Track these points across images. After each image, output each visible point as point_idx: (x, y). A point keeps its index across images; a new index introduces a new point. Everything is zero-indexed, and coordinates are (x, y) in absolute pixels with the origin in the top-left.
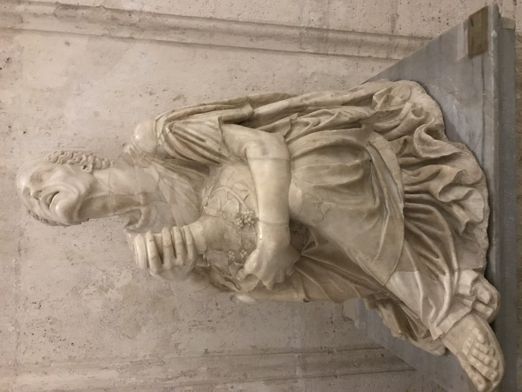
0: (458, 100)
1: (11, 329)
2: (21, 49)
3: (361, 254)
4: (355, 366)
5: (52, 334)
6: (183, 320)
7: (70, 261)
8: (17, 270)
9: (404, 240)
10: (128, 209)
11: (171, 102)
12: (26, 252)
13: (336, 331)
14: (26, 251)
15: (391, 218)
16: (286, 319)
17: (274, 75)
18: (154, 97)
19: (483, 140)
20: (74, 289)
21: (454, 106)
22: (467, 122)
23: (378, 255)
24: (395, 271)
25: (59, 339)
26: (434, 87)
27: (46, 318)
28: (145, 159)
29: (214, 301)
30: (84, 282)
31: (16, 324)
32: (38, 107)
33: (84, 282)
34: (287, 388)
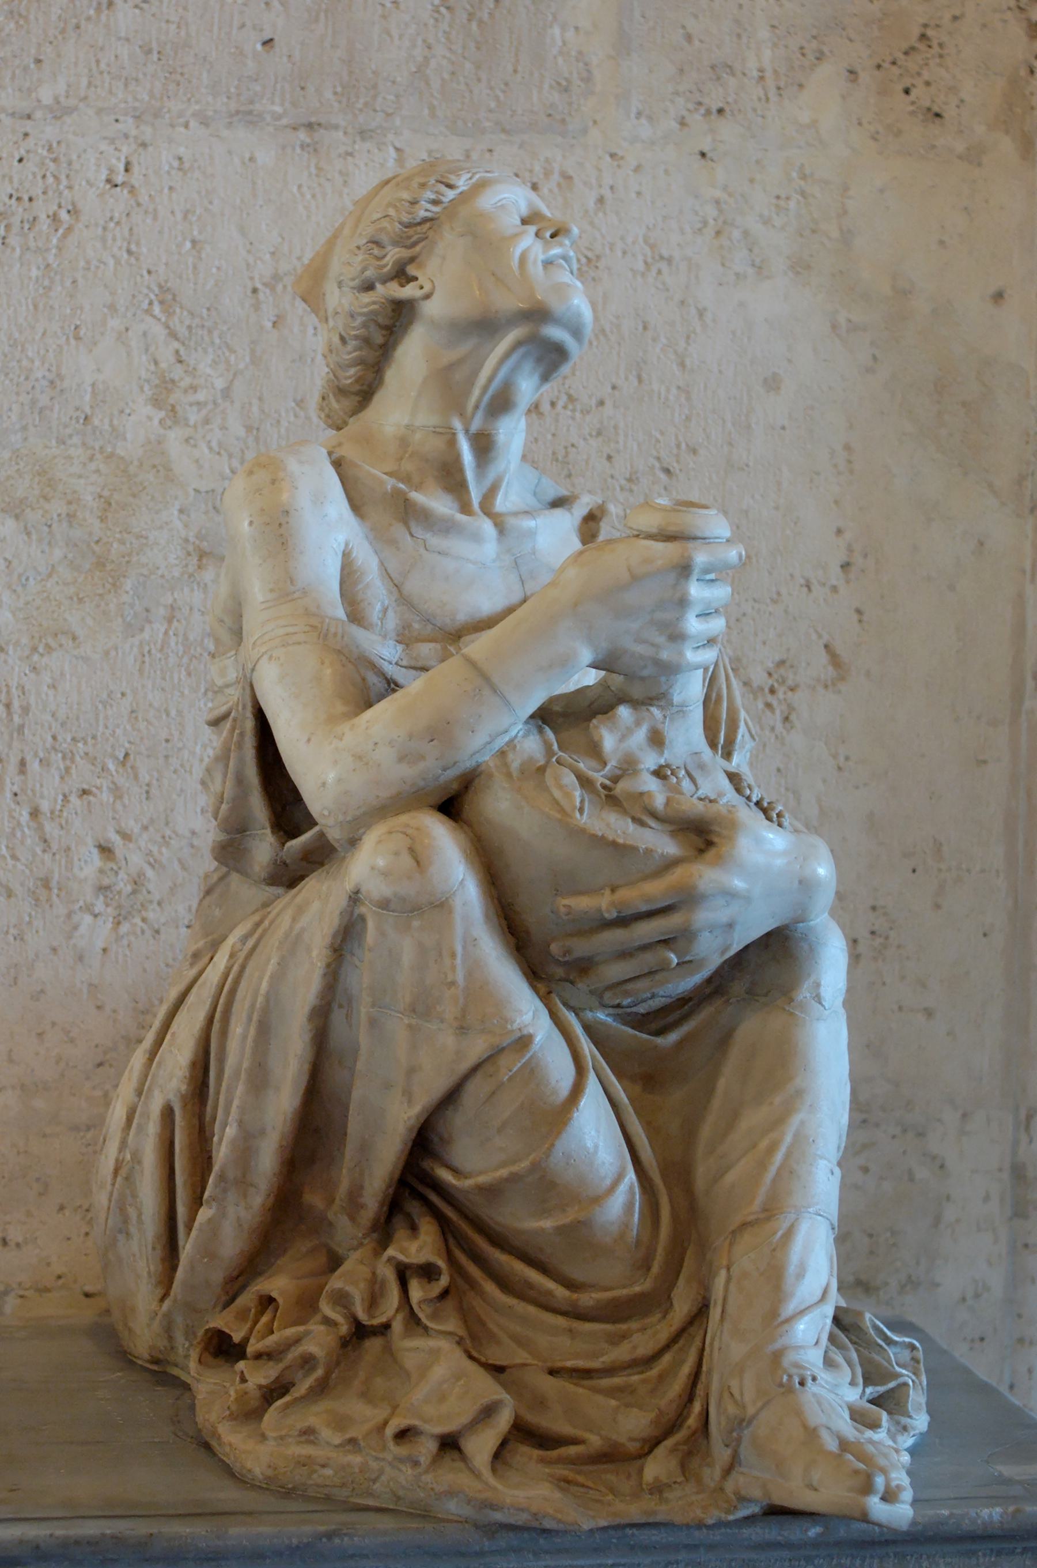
1: (46, 95)
2: (974, 156)
5: (16, 220)
8: (247, 116)
10: (467, 456)
11: (820, 636)
14: (312, 148)
16: (11, 1061)
17: (929, 1013)
18: (835, 576)
31: (59, 111)
32: (788, 198)
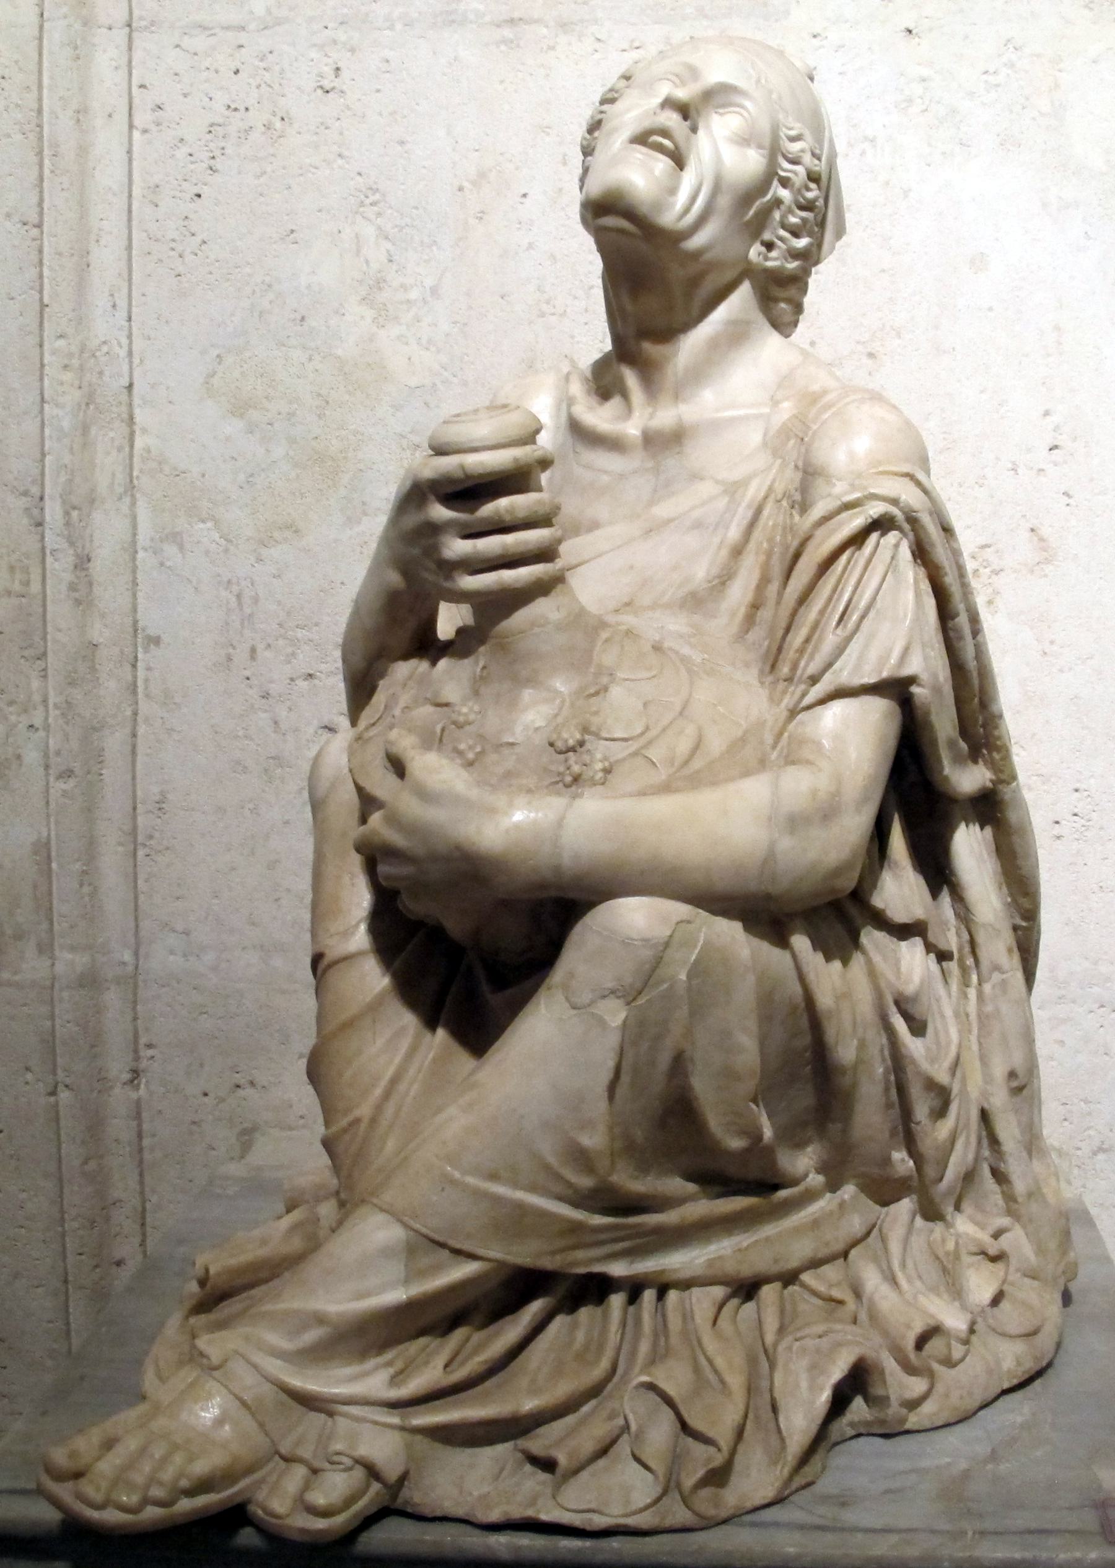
4: (85, 1162)
6: (259, 560)
7: (474, 183)
9: (501, 1264)
12: (505, 41)
13: (206, 1099)
15: (576, 1228)
20: (377, 197)
21: (948, 1460)
23: (457, 1175)
24: (406, 1226)
25: (217, 153)
26: (1026, 1410)
27: (287, 112)
29: (323, 667)
30: (401, 228)
33: (401, 228)
34: (21, 919)
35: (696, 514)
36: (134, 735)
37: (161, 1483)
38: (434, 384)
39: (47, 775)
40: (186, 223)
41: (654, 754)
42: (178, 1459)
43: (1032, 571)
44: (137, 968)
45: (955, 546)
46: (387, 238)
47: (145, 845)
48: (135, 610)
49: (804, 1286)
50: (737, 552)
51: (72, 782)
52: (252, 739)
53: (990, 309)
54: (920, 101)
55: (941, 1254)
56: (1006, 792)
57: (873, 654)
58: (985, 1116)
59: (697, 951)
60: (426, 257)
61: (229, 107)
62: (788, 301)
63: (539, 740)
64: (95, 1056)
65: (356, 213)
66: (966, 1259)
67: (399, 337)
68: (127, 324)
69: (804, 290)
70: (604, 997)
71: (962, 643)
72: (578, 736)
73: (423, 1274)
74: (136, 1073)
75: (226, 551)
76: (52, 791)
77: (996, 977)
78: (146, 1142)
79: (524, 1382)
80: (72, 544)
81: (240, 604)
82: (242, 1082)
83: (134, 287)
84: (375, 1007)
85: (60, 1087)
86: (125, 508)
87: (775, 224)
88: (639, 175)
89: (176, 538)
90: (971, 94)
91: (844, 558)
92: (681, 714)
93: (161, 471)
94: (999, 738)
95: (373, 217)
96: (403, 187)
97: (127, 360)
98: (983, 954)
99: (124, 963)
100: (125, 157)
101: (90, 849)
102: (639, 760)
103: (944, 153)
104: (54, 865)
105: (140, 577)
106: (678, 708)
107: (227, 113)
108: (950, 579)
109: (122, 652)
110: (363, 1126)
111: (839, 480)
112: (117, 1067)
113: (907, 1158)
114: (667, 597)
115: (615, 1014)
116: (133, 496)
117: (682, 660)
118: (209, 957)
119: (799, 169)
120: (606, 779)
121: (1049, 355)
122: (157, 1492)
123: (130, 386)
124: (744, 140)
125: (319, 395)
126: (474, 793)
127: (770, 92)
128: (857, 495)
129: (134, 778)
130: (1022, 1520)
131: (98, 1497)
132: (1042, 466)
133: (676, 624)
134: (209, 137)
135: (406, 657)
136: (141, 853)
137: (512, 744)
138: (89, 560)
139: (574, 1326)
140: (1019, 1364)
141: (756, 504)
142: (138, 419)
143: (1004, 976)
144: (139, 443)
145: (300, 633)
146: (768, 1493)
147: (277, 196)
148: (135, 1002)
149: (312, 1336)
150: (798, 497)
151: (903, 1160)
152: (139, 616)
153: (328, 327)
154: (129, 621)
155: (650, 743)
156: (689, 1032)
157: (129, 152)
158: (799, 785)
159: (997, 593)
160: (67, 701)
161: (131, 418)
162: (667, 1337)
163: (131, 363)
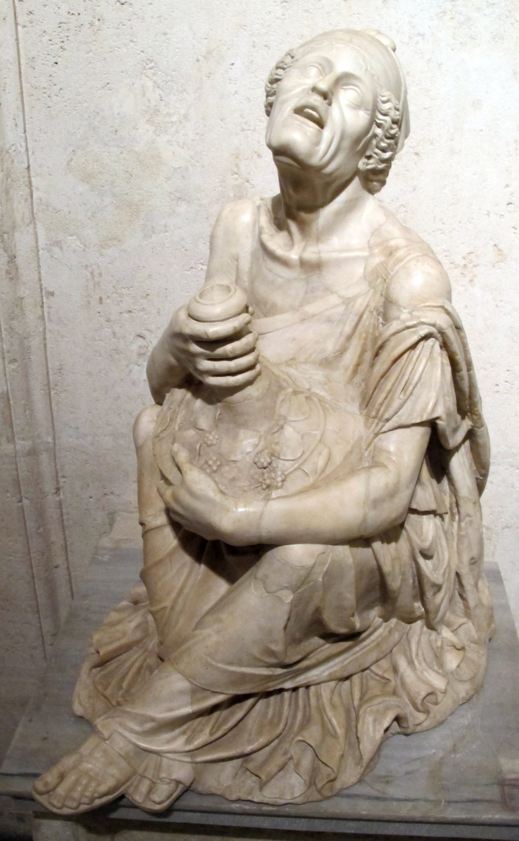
0: (442, 758)
3: (215, 638)
4: (38, 529)
6: (101, 255)
7: (205, 57)
13: (91, 500)
19: (377, 798)
21: (434, 751)
22: (407, 773)
23: (214, 663)
24: (190, 682)
25: (65, 39)
26: (469, 716)
28: (378, 277)
30: (167, 82)
33: (167, 82)
35: (328, 313)
36: (45, 339)
37: (86, 797)
38: (187, 167)
39: (4, 362)
40: (51, 78)
41: (307, 468)
42: (93, 784)
43: (494, 266)
44: (55, 444)
45: (462, 334)
46: (159, 87)
47: (54, 389)
48: (40, 280)
49: (372, 671)
50: (349, 338)
51: (16, 364)
52: (102, 341)
53: (481, 130)
54: (449, 12)
55: (434, 647)
56: (479, 432)
57: (419, 407)
58: (457, 575)
59: (327, 566)
60: (180, 98)
61: (69, 13)
62: (378, 181)
63: (249, 460)
64: (38, 484)
65: (142, 73)
66: (446, 648)
67: (169, 141)
68: (23, 135)
69: (387, 175)
70: (282, 589)
71: (462, 382)
72: (269, 460)
73: (199, 701)
74: (58, 489)
75: (84, 250)
76: (7, 369)
77: (468, 519)
78: (65, 517)
79: (246, 736)
80: (6, 251)
81: (93, 277)
82: (108, 492)
83: (26, 114)
84: (171, 554)
85: (23, 498)
86: (31, 229)
87: (373, 146)
88: (299, 135)
89: (58, 243)
90: (478, 9)
91: (406, 356)
92: (320, 441)
93: (48, 210)
94: (477, 411)
95: (150, 75)
96: (166, 59)
97: (25, 154)
98: (463, 510)
99: (48, 443)
100: (15, 42)
101: (28, 391)
102: (299, 473)
103: (461, 43)
104: (11, 402)
105: (42, 263)
106: (318, 437)
107: (68, 16)
108: (460, 357)
109: (35, 300)
110: (168, 610)
111: (405, 308)
112: (49, 487)
113: (421, 606)
114: (312, 357)
115: (288, 597)
116: (35, 223)
117: (320, 401)
118: (89, 438)
119: (388, 119)
120: (283, 485)
121: (511, 155)
122: (85, 800)
123: (29, 167)
124: (357, 106)
125: (127, 172)
126: (218, 498)
127: (373, 75)
128: (415, 322)
129: (46, 359)
130: (466, 793)
131: (59, 805)
132: (503, 213)
133: (318, 374)
134: (59, 29)
135: (180, 387)
136: (53, 392)
137: (235, 461)
138: (15, 257)
139: (268, 706)
140: (467, 694)
141: (360, 314)
142: (34, 183)
143: (471, 519)
144: (35, 196)
145: (125, 291)
146: (354, 780)
147: (99, 64)
148: (55, 459)
149: (149, 726)
150: (382, 310)
151: (419, 607)
152: (43, 282)
153: (130, 136)
154: (38, 286)
155: (305, 461)
156: (323, 600)
157: (17, 40)
158: (379, 481)
159: (475, 276)
160: (10, 328)
161: (30, 183)
162: (310, 708)
163: (28, 155)
